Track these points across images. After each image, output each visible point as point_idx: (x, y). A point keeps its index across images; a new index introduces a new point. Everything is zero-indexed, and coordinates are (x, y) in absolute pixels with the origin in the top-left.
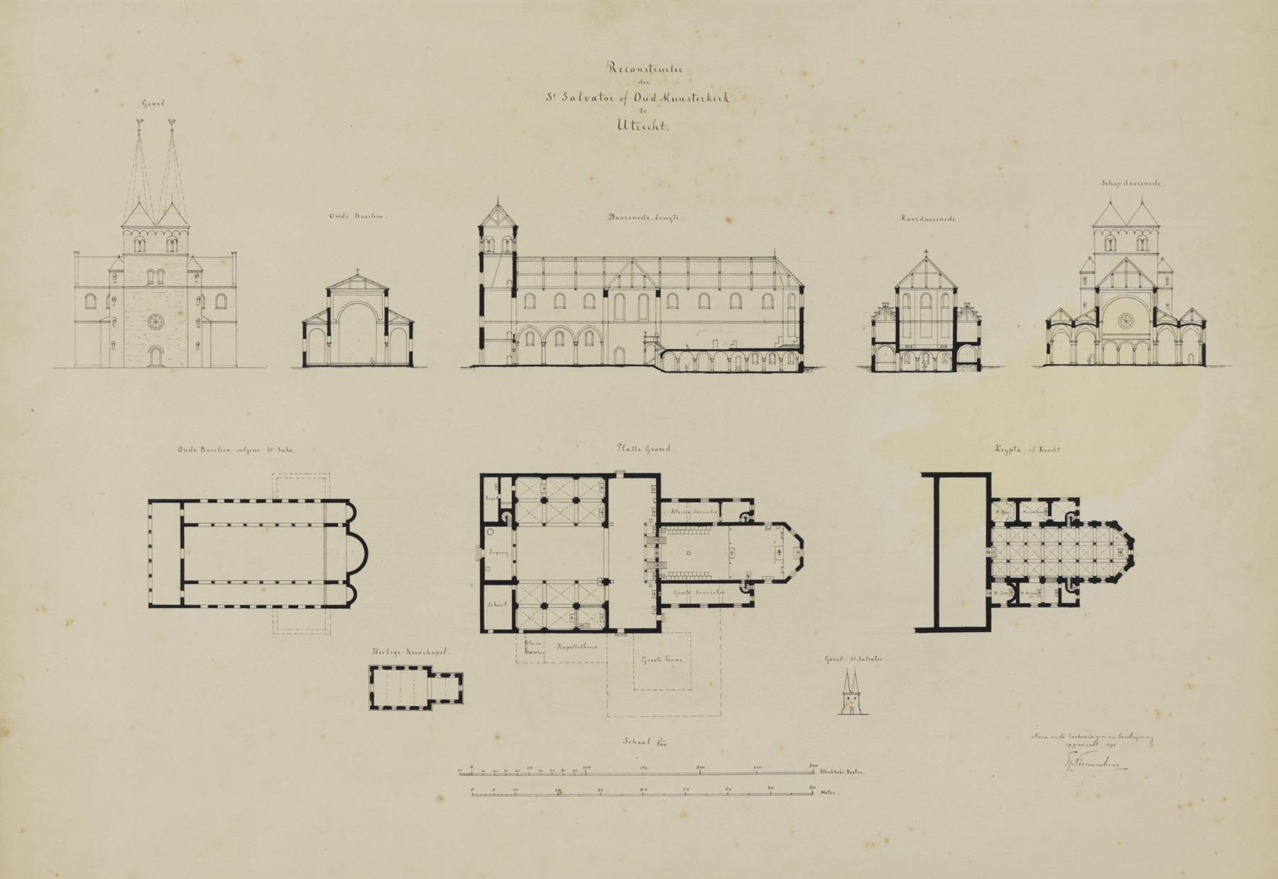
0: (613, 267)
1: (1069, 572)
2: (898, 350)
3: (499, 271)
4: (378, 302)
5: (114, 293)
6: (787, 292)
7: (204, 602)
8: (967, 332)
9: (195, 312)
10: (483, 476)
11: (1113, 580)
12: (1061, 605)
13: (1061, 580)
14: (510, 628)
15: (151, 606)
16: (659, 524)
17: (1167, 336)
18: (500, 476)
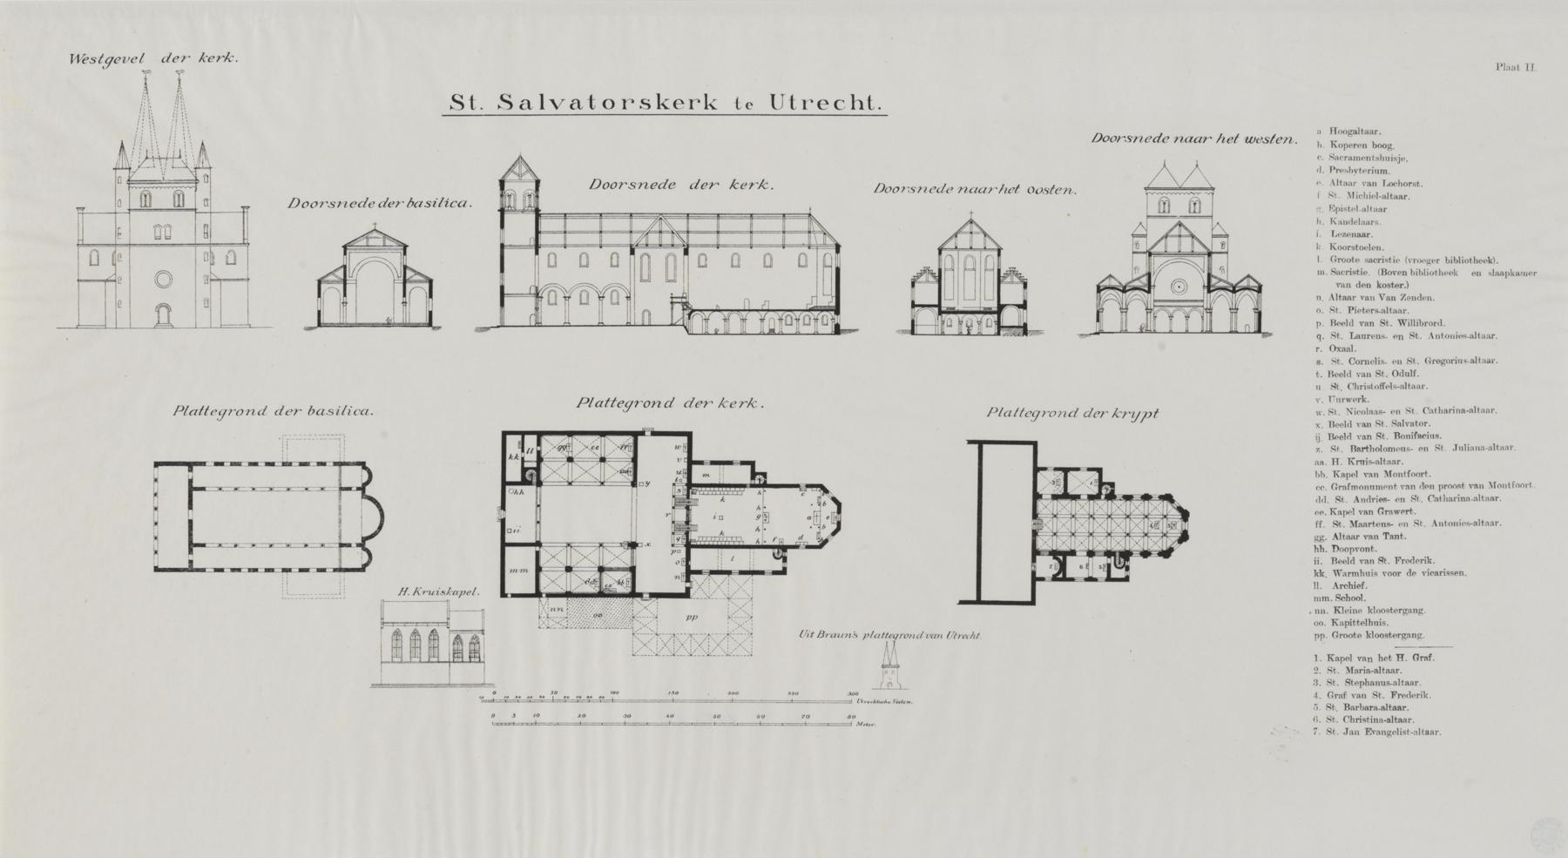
0: (640, 224)
1: (1118, 545)
2: (941, 313)
3: (520, 227)
4: (395, 258)
5: (119, 250)
6: (821, 252)
7: (210, 565)
8: (1012, 294)
9: (204, 268)
10: (505, 434)
11: (1166, 554)
12: (1109, 579)
13: (1109, 554)
14: (533, 591)
15: (157, 569)
16: (690, 485)
17: (1222, 301)
18: (523, 434)
